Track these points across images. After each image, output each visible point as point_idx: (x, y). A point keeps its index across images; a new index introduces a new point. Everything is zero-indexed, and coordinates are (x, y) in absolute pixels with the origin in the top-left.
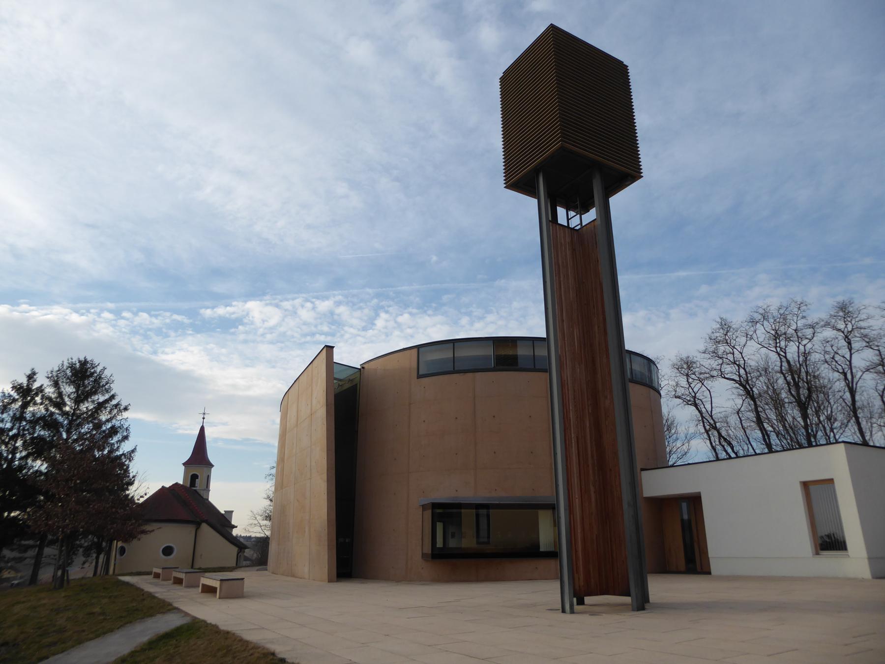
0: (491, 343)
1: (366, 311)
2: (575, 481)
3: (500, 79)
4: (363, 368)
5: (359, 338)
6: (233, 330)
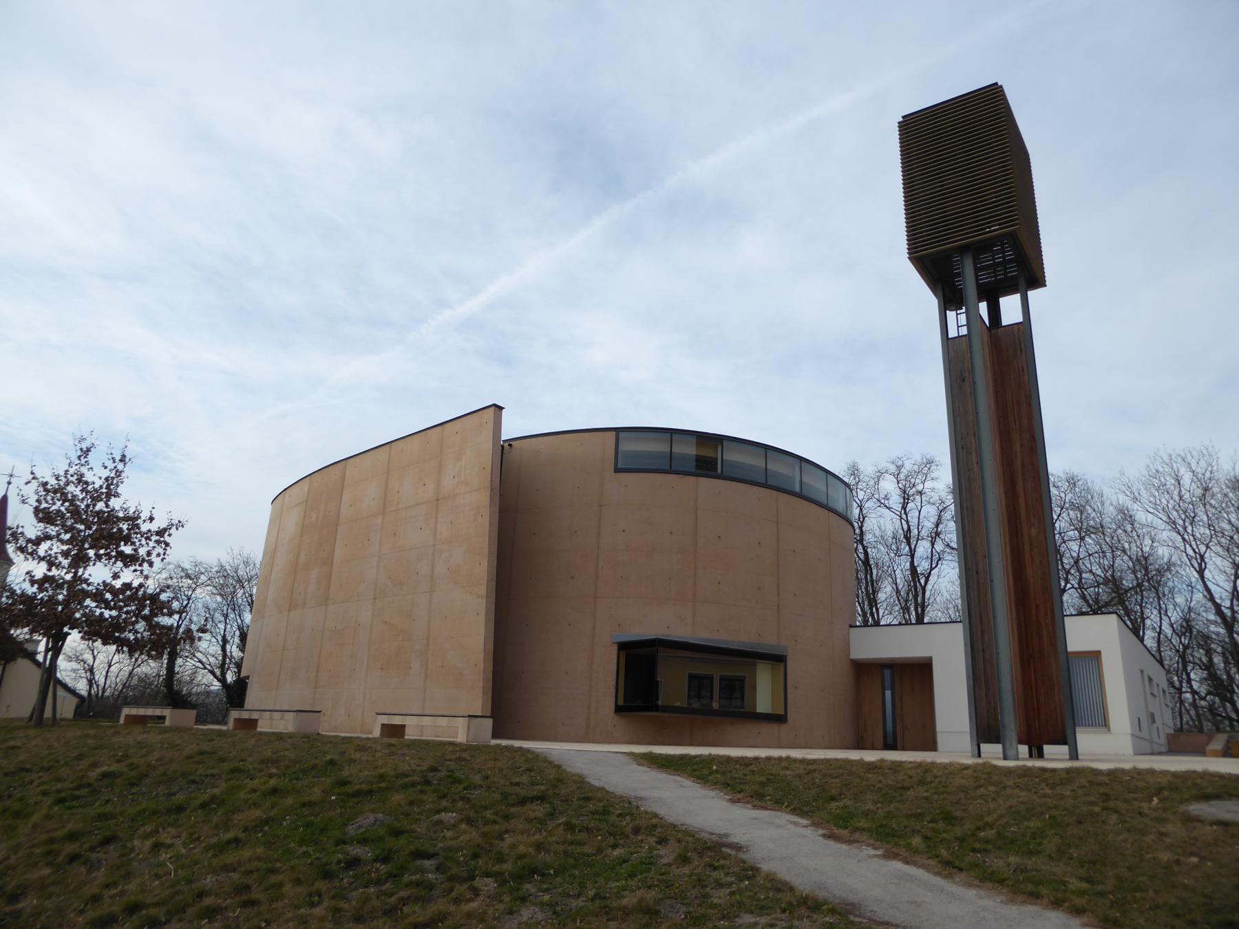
0: (693, 439)
3: (903, 117)
4: (510, 445)
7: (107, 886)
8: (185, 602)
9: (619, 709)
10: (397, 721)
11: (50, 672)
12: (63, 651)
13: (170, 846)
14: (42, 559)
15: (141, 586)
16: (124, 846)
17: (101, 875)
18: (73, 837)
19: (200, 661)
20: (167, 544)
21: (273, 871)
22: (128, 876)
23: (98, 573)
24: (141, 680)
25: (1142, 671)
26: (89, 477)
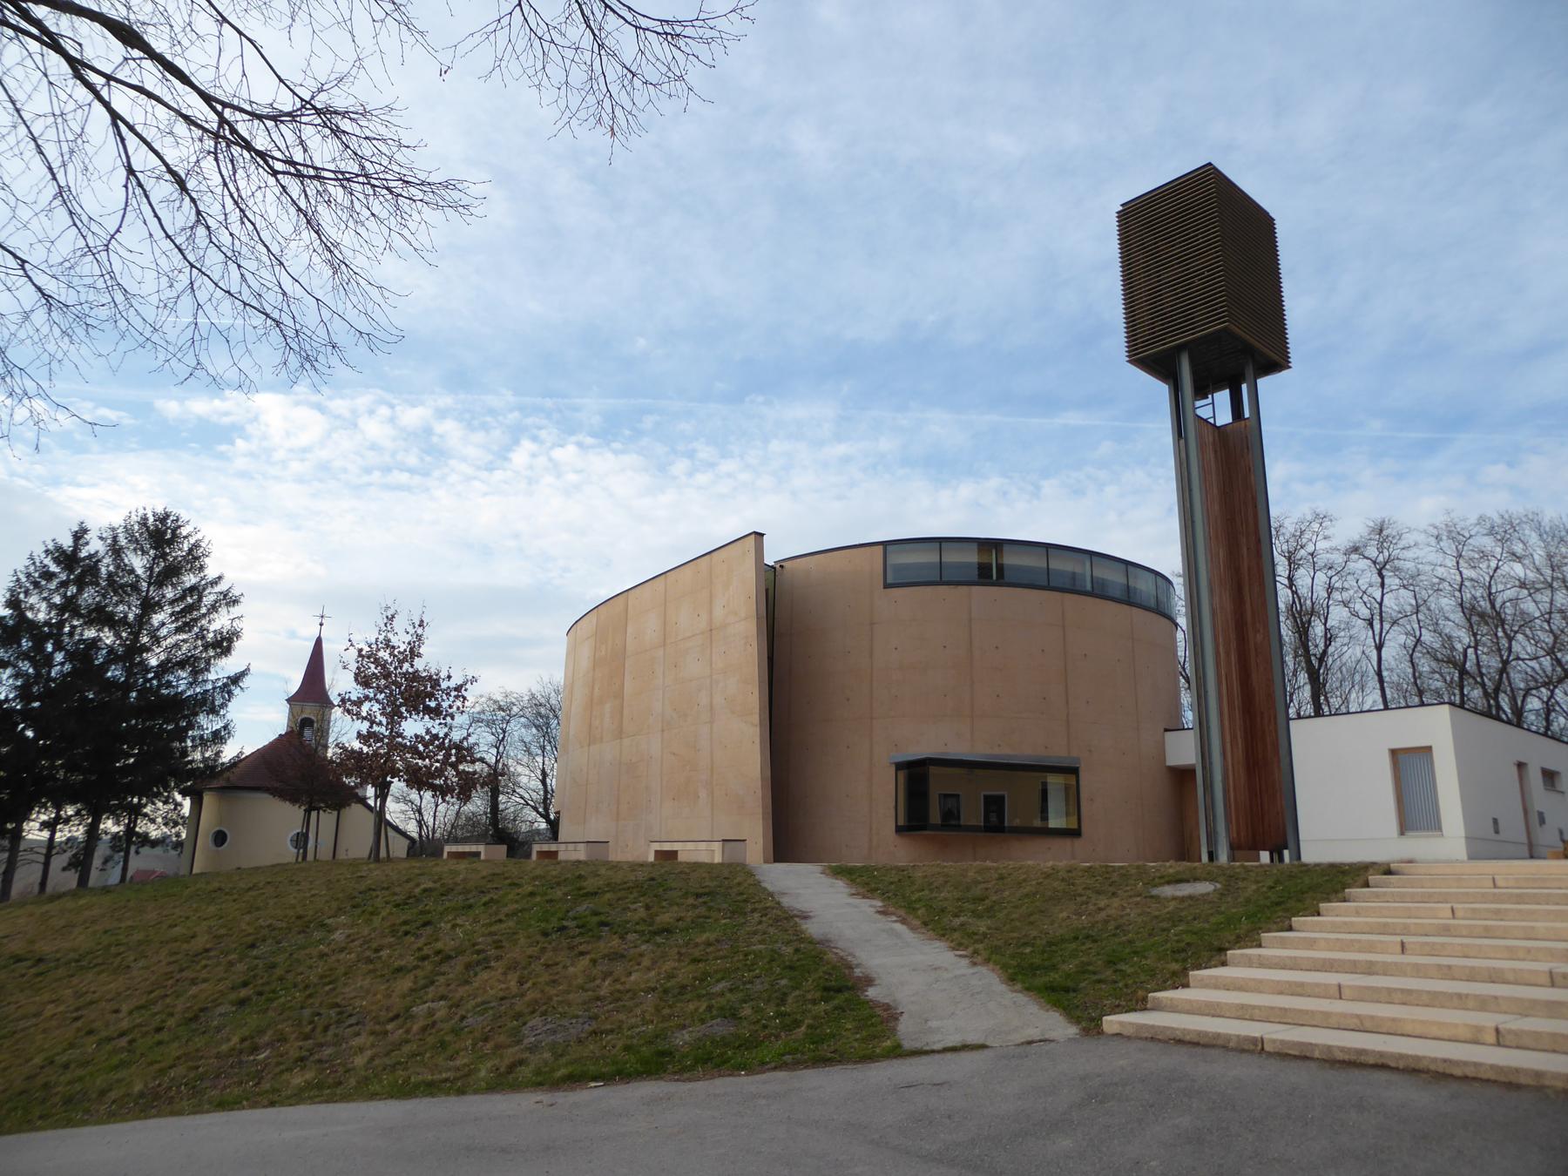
0: (975, 546)
1: (497, 433)
2: (1226, 723)
3: (1122, 205)
4: (781, 566)
5: (477, 484)
6: (223, 448)
7: (426, 945)
8: (501, 736)
9: (899, 830)
10: (667, 847)
11: (380, 814)
12: (390, 793)
13: (461, 926)
14: (364, 718)
15: (446, 735)
16: (436, 927)
17: (422, 941)
18: (405, 923)
19: (522, 798)
20: (465, 698)
21: (514, 933)
22: (437, 940)
23: (413, 727)
24: (468, 819)
25: (1521, 766)
26: (395, 641)
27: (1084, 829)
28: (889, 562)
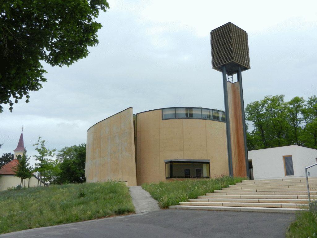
3: (212, 31)
9: (167, 178)
27: (211, 176)
28: (163, 113)
